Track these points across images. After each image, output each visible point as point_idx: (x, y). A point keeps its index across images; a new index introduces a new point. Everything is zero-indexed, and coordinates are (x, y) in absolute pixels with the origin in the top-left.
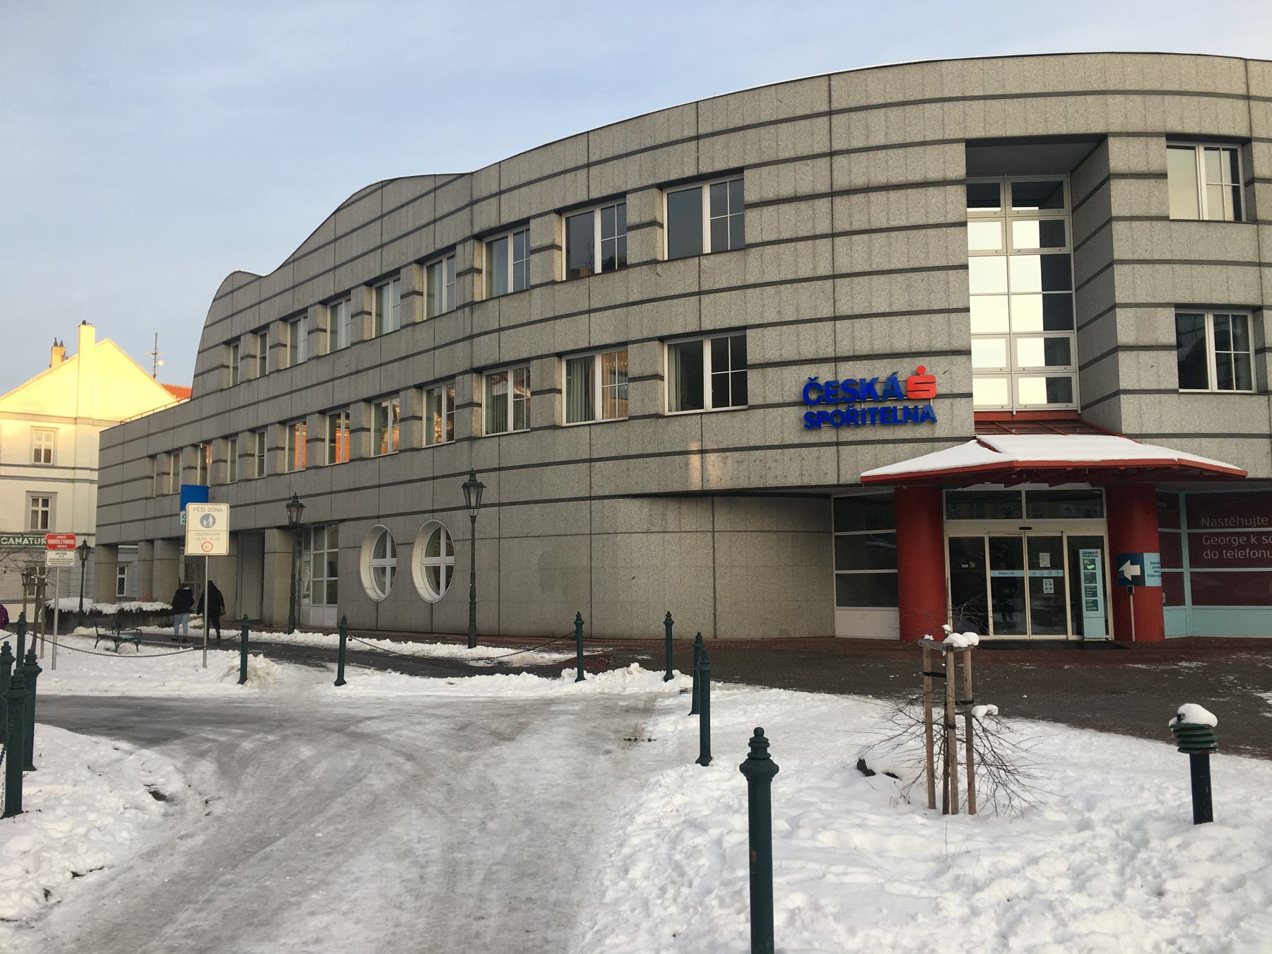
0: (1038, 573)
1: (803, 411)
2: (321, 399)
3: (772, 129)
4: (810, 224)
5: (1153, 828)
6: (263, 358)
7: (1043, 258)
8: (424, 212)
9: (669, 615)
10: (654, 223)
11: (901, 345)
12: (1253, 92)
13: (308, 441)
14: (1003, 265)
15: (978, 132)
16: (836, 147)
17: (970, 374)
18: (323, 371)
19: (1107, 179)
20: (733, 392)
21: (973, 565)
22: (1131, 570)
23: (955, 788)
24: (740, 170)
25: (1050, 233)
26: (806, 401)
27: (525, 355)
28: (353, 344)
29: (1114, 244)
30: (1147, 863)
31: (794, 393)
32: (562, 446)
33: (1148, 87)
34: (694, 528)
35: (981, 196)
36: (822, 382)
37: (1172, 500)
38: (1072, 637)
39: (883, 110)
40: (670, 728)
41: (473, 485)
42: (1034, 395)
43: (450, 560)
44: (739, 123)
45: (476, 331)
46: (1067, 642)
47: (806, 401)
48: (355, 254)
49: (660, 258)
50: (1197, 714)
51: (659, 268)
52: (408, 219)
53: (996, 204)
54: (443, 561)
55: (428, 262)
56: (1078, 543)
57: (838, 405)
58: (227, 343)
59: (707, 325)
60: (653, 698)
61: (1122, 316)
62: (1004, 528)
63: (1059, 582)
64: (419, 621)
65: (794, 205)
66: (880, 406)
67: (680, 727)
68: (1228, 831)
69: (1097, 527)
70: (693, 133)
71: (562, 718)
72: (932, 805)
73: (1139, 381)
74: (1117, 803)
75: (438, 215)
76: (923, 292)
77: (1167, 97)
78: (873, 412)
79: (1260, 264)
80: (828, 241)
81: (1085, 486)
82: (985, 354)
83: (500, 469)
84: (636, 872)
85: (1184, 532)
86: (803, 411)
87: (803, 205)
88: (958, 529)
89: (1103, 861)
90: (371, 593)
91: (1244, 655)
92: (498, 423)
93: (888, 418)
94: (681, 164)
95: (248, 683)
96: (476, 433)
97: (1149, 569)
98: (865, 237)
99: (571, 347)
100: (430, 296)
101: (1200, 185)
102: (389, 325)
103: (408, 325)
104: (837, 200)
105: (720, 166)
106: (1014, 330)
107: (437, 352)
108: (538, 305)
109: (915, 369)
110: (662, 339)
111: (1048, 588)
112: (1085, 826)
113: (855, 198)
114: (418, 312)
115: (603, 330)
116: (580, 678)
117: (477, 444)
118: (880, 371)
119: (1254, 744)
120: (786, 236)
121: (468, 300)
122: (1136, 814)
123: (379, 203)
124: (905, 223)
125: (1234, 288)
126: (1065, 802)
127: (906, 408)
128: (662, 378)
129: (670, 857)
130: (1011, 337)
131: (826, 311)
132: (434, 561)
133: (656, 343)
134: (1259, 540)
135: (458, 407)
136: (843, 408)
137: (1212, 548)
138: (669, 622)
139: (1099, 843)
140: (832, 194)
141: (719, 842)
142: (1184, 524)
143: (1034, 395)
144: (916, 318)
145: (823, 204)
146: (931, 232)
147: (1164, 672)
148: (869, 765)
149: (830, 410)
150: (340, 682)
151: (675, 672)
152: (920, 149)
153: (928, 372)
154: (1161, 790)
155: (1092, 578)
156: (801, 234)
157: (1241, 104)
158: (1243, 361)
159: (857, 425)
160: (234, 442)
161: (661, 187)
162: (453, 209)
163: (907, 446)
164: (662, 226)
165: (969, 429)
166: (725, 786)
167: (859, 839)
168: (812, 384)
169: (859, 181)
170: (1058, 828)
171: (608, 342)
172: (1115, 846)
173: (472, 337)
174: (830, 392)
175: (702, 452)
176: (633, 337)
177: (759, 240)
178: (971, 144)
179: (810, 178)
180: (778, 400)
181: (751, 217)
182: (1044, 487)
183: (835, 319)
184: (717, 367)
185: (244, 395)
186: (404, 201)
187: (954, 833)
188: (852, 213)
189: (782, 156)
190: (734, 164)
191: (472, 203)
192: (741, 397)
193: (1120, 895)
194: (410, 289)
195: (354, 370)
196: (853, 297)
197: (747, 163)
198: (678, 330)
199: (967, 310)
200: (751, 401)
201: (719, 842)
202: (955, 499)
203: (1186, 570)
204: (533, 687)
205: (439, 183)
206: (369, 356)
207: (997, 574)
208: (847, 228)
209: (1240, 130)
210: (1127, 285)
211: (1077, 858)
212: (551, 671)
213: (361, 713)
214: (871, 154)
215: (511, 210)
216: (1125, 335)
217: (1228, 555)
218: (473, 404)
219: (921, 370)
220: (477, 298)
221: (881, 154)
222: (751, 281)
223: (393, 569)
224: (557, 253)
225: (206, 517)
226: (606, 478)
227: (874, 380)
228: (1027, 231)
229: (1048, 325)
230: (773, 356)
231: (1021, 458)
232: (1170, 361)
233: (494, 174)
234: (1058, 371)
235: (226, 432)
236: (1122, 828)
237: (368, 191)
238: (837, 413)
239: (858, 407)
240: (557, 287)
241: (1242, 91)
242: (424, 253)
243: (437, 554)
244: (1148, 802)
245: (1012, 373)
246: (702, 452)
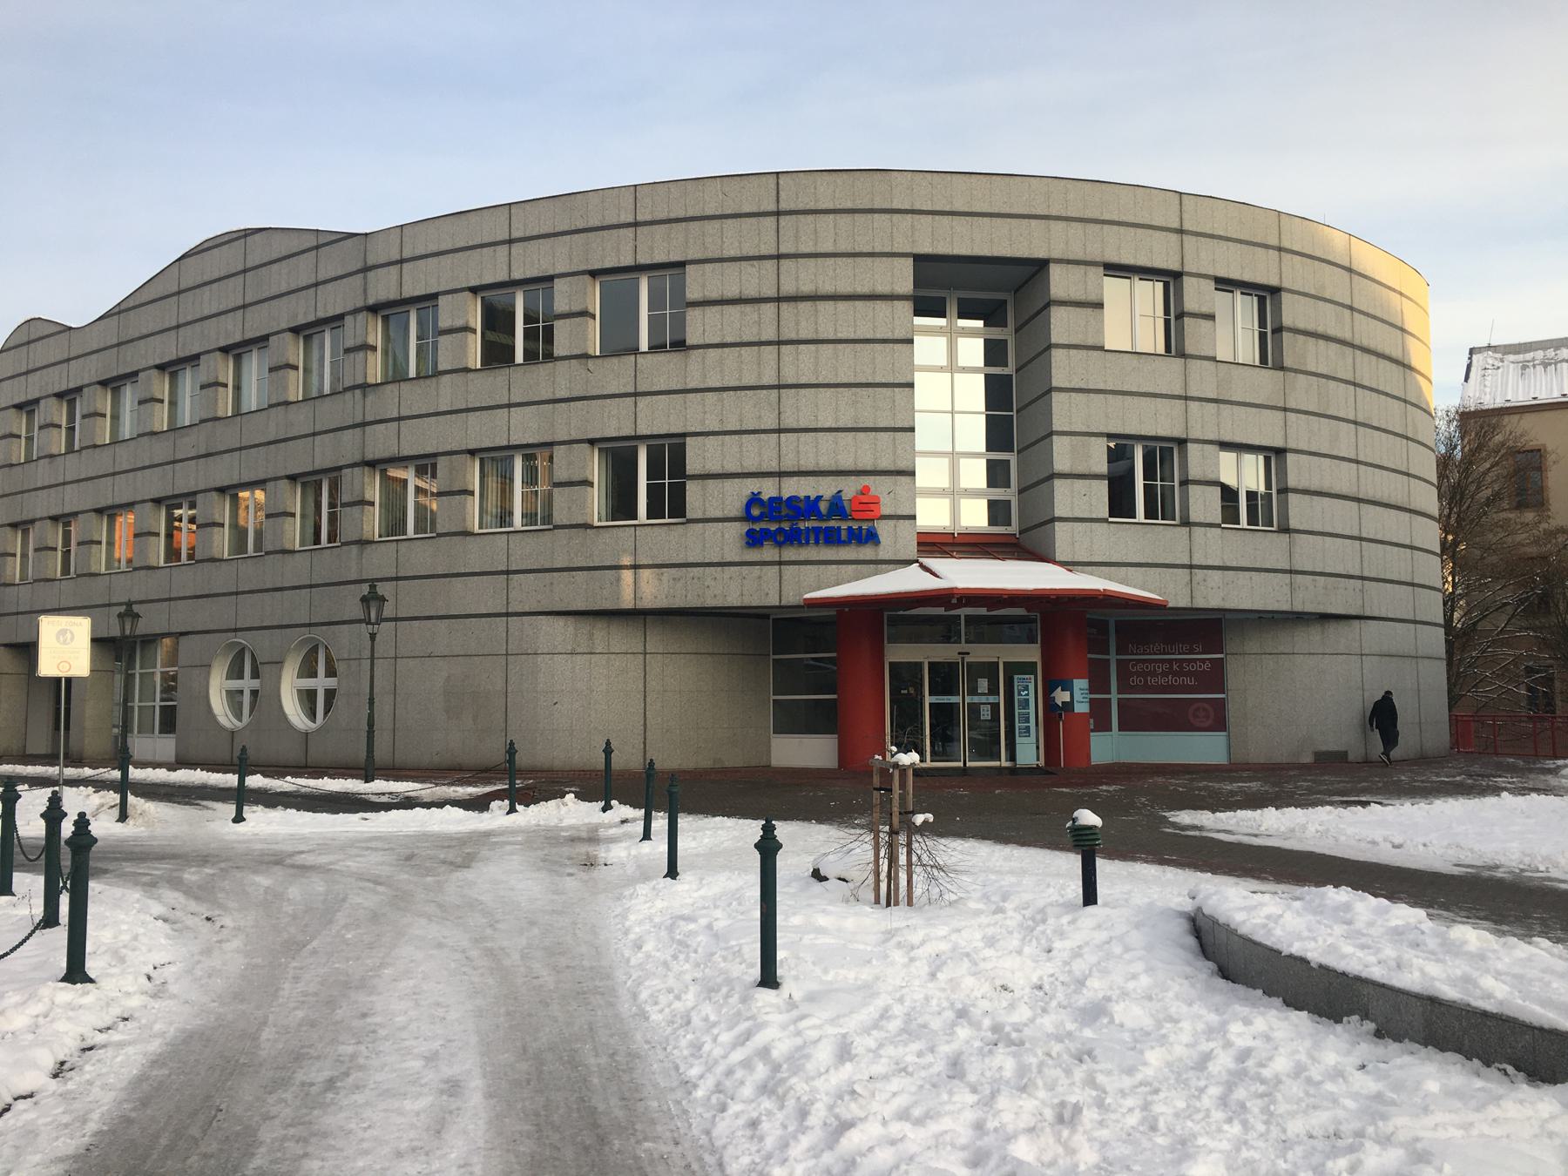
0: (976, 699)
1: (744, 527)
2: (154, 484)
3: (716, 224)
4: (755, 330)
5: (1049, 910)
6: (71, 430)
7: (987, 376)
8: (302, 271)
9: (608, 743)
10: (585, 314)
11: (846, 463)
12: (1186, 227)
13: (136, 536)
14: (947, 378)
15: (926, 248)
16: (783, 250)
17: (913, 494)
18: (160, 450)
19: (1048, 305)
20: (670, 503)
21: (912, 691)
22: (1062, 696)
23: (897, 889)
24: (681, 265)
25: (994, 353)
26: (748, 517)
27: (429, 450)
28: (203, 421)
29: (1054, 371)
30: (1043, 932)
31: (735, 506)
32: (473, 556)
33: (1089, 214)
34: (624, 649)
35: (927, 306)
36: (765, 497)
37: (1102, 627)
38: (1005, 763)
39: (832, 216)
40: (623, 854)
41: (372, 599)
42: (975, 516)
43: (331, 683)
44: (682, 214)
45: (369, 418)
46: (1000, 769)
47: (748, 517)
48: (206, 312)
49: (591, 352)
50: (1088, 817)
51: (590, 363)
52: (280, 278)
53: (941, 314)
54: (321, 683)
55: (305, 331)
56: (1013, 669)
57: (780, 522)
58: (19, 407)
59: (643, 430)
60: (594, 829)
61: (1059, 444)
62: (944, 653)
63: (995, 707)
64: (292, 754)
65: (738, 307)
66: (824, 525)
67: (633, 852)
68: (1107, 911)
69: (1031, 653)
70: (630, 219)
71: (508, 848)
72: (877, 901)
73: (1072, 509)
74: (1027, 897)
75: (321, 278)
76: (870, 408)
77: (1106, 227)
78: (817, 530)
79: (1186, 398)
80: (773, 349)
81: (1020, 611)
82: (929, 473)
83: (397, 579)
84: (649, 947)
85: (1113, 658)
86: (744, 527)
87: (748, 308)
88: (899, 653)
89: (1011, 933)
90: (223, 720)
91: (1160, 780)
92: (395, 525)
93: (831, 538)
94: (617, 251)
95: (130, 821)
96: (366, 536)
97: (1078, 695)
98: (812, 347)
99: (487, 444)
100: (307, 371)
101: (1130, 317)
102: (251, 401)
103: (279, 404)
104: (784, 306)
105: (660, 258)
106: (958, 449)
107: (318, 438)
108: (447, 393)
109: (860, 488)
110: (592, 442)
111: (986, 714)
112: (1000, 910)
113: (802, 306)
114: (292, 388)
115: (525, 427)
116: (512, 810)
117: (369, 549)
118: (825, 488)
119: (1148, 853)
120: (729, 339)
121: (360, 381)
122: (1041, 903)
123: (240, 254)
124: (852, 336)
125: (1160, 421)
126: (986, 897)
127: (850, 529)
128: (591, 484)
129: (673, 939)
130: (954, 456)
131: (771, 423)
132: (308, 683)
133: (586, 445)
134: (1180, 667)
135: (344, 505)
136: (786, 526)
137: (1138, 674)
138: (608, 751)
139: (1008, 922)
140: (778, 299)
141: (709, 927)
142: (1113, 649)
143: (975, 516)
144: (861, 435)
145: (769, 309)
146: (878, 346)
147: (1085, 794)
148: (823, 873)
149: (773, 527)
150: (239, 819)
151: (614, 802)
152: (869, 260)
153: (873, 492)
154: (1063, 887)
155: (1025, 704)
156: (746, 339)
157: (1174, 237)
158: (1168, 493)
159: (800, 544)
160: (25, 533)
161: (594, 274)
162: (340, 273)
163: (851, 567)
164: (593, 317)
165: (911, 550)
166: (695, 895)
167: (822, 921)
168: (754, 500)
169: (806, 288)
170: (977, 913)
171: (531, 441)
172: (1021, 925)
173: (364, 424)
174: (773, 508)
175: (635, 567)
176: (562, 436)
177: (701, 342)
178: (919, 259)
179: (755, 280)
180: (719, 514)
181: (694, 316)
182: (983, 611)
183: (779, 431)
184: (651, 476)
185: (43, 473)
186: (275, 256)
187: (897, 917)
188: (800, 320)
189: (726, 254)
190: (675, 257)
191: (366, 269)
192: (679, 510)
193: (1019, 952)
194: (282, 361)
195: (203, 452)
196: (800, 409)
197: (689, 258)
198: (611, 432)
199: (912, 430)
200: (689, 515)
201: (709, 927)
202: (893, 621)
203: (1114, 697)
204: (460, 821)
205: (322, 240)
206: (226, 437)
207: (935, 699)
208: (793, 336)
209: (1174, 265)
210: (1065, 412)
211: (990, 931)
212: (478, 804)
213: (289, 848)
214: (820, 260)
215: (416, 282)
216: (1061, 463)
217: (1152, 681)
218: (364, 503)
219: (866, 490)
220: (371, 380)
221: (830, 261)
222: (691, 386)
223: (254, 693)
224: (470, 336)
225: (63, 632)
226: (527, 592)
227: (819, 498)
228: (972, 351)
229: (990, 446)
230: (714, 467)
231: (960, 586)
232: (1101, 489)
233: (395, 237)
234: (999, 494)
235: (17, 519)
236: (1028, 913)
237: (226, 238)
238: (780, 530)
239: (802, 526)
240: (471, 375)
241: (1176, 225)
242: (301, 320)
243: (314, 675)
244: (1052, 895)
245: (954, 493)
246: (635, 567)
